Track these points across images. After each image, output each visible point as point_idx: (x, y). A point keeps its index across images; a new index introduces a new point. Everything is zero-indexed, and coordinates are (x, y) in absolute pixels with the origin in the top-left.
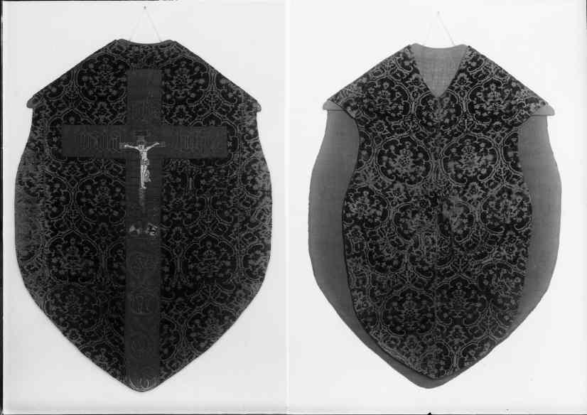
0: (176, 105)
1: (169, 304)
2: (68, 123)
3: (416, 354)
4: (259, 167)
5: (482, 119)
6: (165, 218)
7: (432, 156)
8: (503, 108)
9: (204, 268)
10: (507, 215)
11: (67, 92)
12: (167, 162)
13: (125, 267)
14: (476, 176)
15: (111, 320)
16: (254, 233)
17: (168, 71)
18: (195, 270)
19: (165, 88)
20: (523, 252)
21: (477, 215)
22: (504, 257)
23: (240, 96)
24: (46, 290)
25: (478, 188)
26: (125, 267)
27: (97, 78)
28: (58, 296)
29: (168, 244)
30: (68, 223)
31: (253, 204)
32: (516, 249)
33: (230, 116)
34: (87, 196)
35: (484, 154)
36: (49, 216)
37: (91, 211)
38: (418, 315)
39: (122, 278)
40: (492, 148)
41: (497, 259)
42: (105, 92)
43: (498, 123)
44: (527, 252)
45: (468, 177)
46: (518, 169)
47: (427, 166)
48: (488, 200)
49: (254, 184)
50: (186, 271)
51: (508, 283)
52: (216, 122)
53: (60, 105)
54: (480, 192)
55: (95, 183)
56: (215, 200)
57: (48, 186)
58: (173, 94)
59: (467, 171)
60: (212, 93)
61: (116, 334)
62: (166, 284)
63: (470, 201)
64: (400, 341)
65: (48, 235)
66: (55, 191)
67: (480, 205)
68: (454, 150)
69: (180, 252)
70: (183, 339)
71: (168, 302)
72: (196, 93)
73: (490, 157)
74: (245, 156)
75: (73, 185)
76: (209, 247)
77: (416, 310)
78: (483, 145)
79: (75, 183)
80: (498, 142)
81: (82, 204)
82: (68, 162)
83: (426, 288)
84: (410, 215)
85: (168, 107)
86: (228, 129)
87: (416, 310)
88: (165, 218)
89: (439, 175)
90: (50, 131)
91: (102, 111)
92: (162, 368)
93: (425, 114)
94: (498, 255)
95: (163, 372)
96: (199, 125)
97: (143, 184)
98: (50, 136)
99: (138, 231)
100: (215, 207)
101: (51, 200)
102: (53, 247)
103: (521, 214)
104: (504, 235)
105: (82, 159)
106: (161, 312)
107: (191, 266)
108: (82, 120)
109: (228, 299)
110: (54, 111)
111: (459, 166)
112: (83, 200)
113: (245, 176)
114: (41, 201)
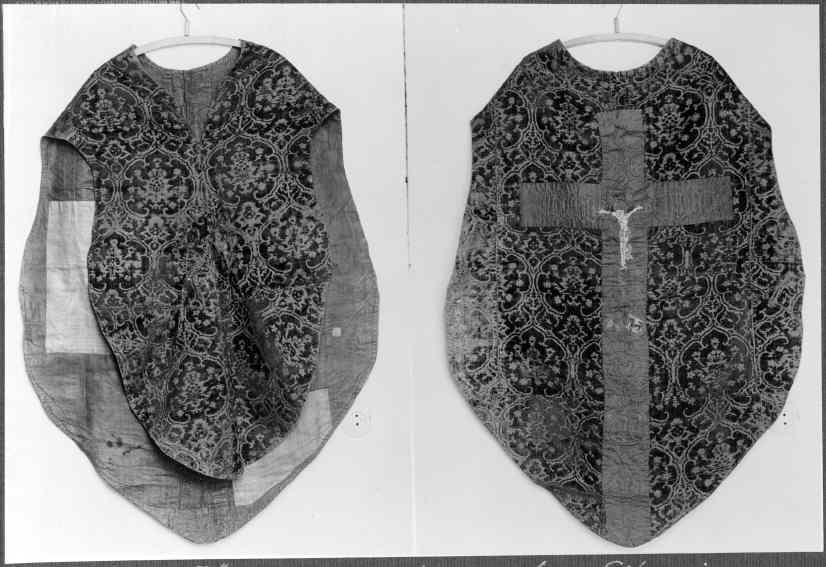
0: (663, 154)
1: (661, 429)
2: (529, 181)
3: (208, 446)
4: (779, 231)
5: (261, 114)
6: (653, 308)
7: (193, 169)
8: (293, 100)
9: (709, 376)
10: (296, 247)
11: (526, 139)
12: (653, 231)
13: (602, 376)
14: (251, 194)
15: (585, 450)
16: (773, 322)
17: (650, 110)
18: (697, 381)
19: (648, 134)
20: (315, 298)
21: (255, 247)
22: (290, 305)
23: (746, 133)
24: (502, 406)
25: (256, 210)
26: (602, 376)
27: (559, 119)
28: (518, 414)
29: (658, 344)
30: (527, 316)
31: (772, 282)
32: (305, 294)
33: (733, 161)
34: (552, 279)
35: (261, 163)
36: (502, 306)
37: (558, 300)
38: (205, 389)
39: (599, 391)
40: (272, 155)
41: (283, 309)
42: (572, 139)
43: (283, 121)
44: (320, 299)
45: (240, 195)
46: (309, 185)
47: (189, 184)
48: (270, 227)
49: (771, 255)
50: (684, 381)
51: (295, 345)
52: (718, 172)
53: (517, 157)
54: (258, 216)
55: (563, 261)
56: (722, 279)
57: (502, 267)
58: (659, 140)
59: (239, 186)
60: (711, 130)
61: (590, 468)
62: (656, 400)
63: (244, 229)
64: (183, 431)
65: (503, 332)
66: (589, 278)
67: (258, 233)
68: (220, 158)
69: (675, 355)
70: (682, 476)
71: (660, 424)
72: (689, 133)
73: (270, 167)
74: (757, 217)
75: (534, 265)
76: (715, 347)
77: (201, 383)
78: (260, 151)
79: (536, 261)
80: (281, 147)
81: (545, 290)
82: (528, 232)
83: (211, 351)
84: (178, 255)
85: (652, 159)
86: (732, 180)
87: (201, 383)
88: (653, 308)
89: (207, 194)
90: (504, 193)
91: (569, 164)
92: (654, 517)
93: (164, 115)
94: (283, 303)
95: (655, 522)
96: (694, 177)
97: (623, 263)
98: (505, 199)
99: (617, 327)
100: (722, 289)
101: (505, 285)
102: (509, 348)
103: (314, 246)
104: (291, 275)
105: (546, 229)
106: (651, 438)
107: (691, 375)
108: (546, 176)
109: (741, 417)
110: (510, 164)
111: (228, 180)
112: (547, 284)
113: (759, 244)
114: (493, 287)
